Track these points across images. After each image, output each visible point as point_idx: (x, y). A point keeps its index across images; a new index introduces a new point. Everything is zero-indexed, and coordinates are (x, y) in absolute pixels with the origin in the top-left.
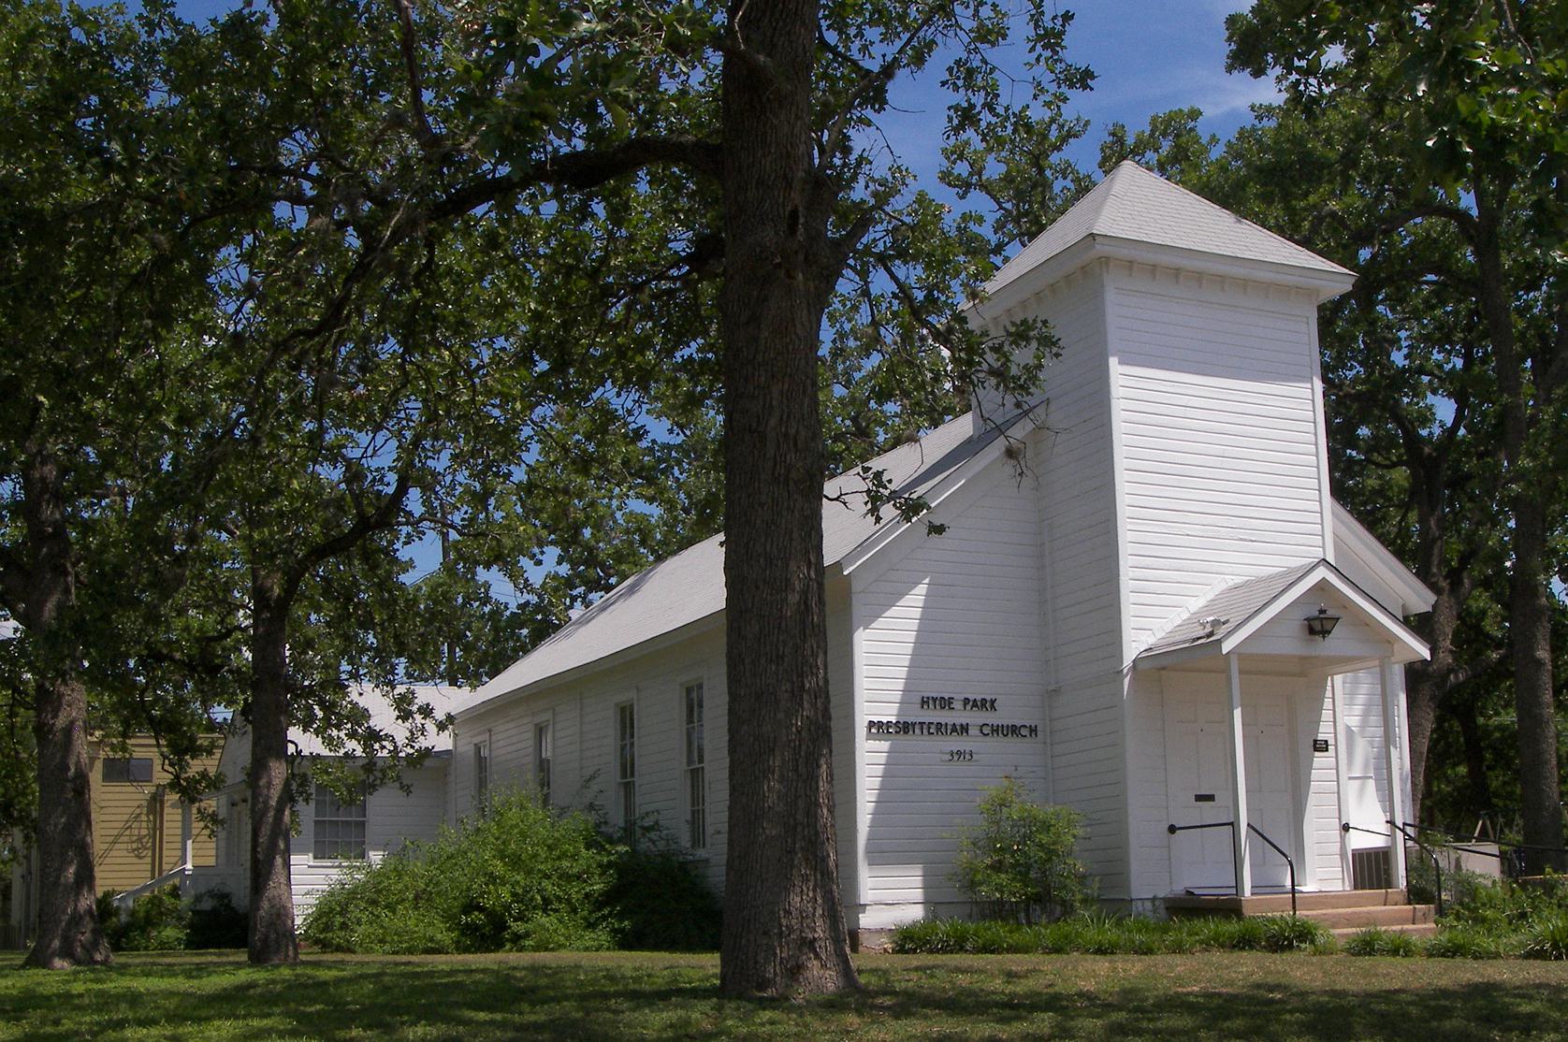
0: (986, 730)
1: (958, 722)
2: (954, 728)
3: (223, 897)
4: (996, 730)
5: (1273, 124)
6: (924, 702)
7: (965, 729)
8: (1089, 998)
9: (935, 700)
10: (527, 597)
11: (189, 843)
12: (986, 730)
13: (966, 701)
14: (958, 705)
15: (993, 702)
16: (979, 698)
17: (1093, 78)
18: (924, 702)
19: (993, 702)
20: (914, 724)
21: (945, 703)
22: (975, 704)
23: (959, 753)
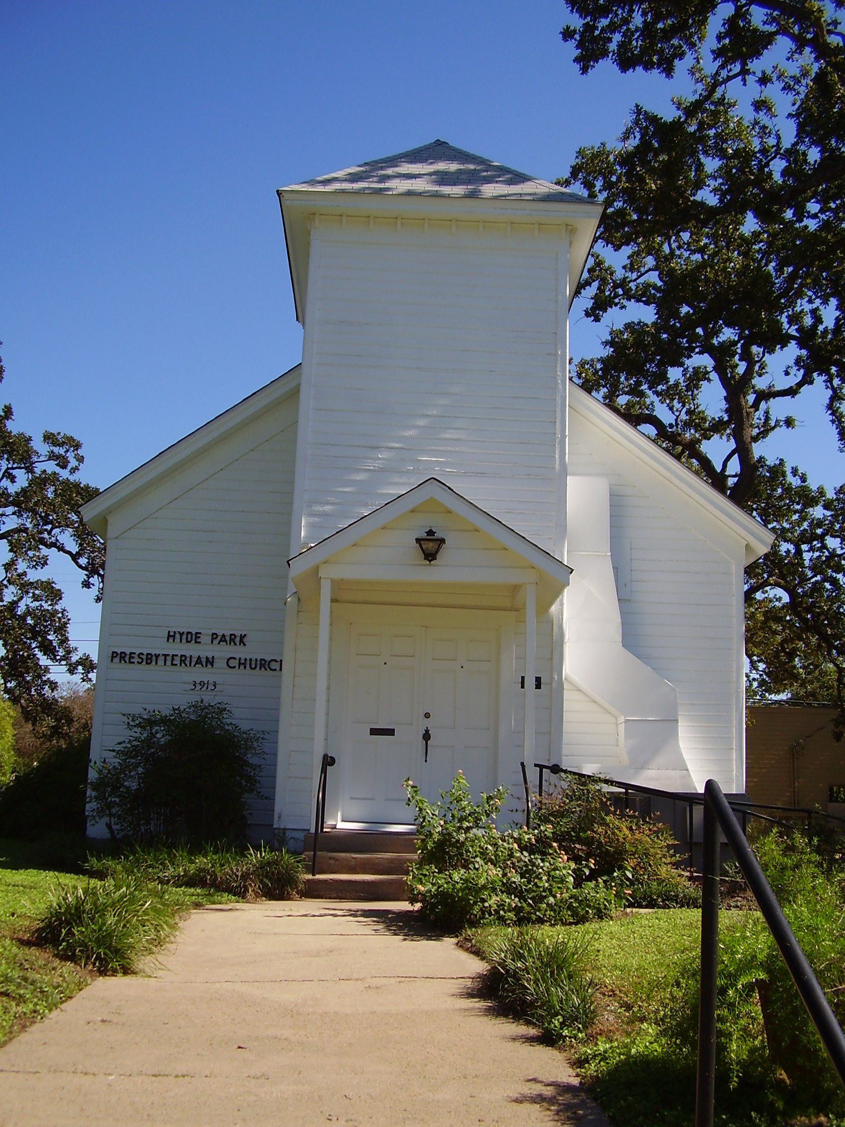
0: (233, 663)
1: (203, 655)
2: (199, 661)
3: (557, 1113)
4: (242, 664)
5: (727, 41)
6: (170, 636)
7: (210, 662)
8: (295, 953)
9: (181, 634)
10: (617, 318)
11: (313, 830)
12: (233, 663)
13: (214, 636)
14: (205, 639)
15: (242, 637)
16: (227, 633)
17: (568, 28)
18: (170, 636)
19: (242, 637)
20: (157, 656)
21: (194, 637)
22: (223, 639)
23: (202, 684)
